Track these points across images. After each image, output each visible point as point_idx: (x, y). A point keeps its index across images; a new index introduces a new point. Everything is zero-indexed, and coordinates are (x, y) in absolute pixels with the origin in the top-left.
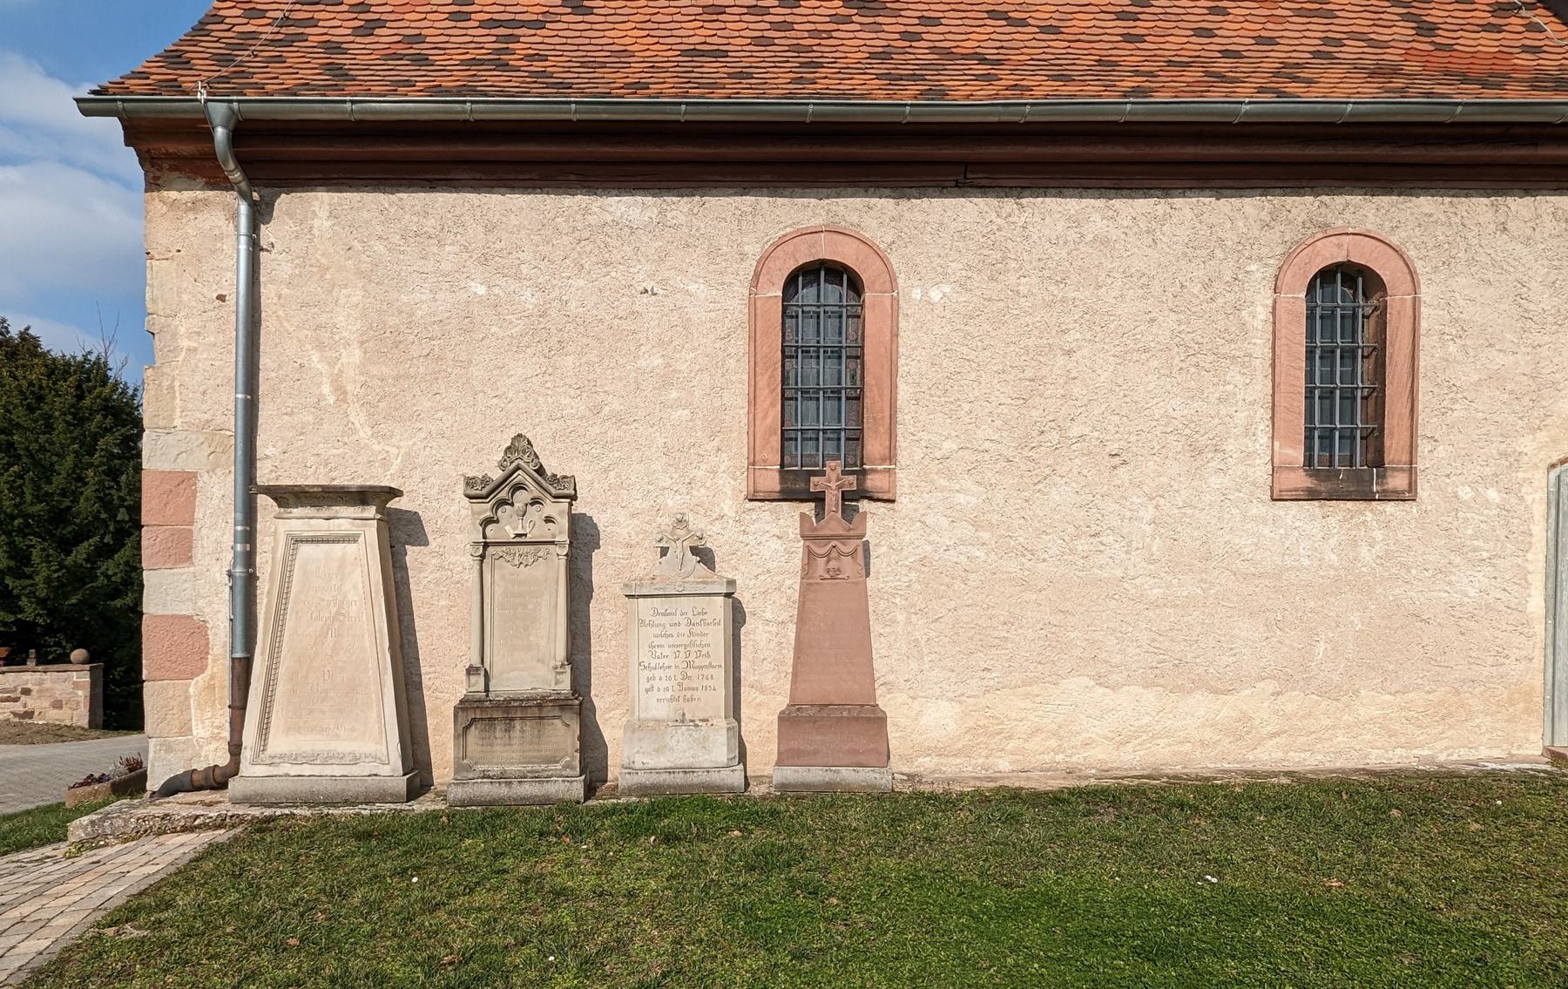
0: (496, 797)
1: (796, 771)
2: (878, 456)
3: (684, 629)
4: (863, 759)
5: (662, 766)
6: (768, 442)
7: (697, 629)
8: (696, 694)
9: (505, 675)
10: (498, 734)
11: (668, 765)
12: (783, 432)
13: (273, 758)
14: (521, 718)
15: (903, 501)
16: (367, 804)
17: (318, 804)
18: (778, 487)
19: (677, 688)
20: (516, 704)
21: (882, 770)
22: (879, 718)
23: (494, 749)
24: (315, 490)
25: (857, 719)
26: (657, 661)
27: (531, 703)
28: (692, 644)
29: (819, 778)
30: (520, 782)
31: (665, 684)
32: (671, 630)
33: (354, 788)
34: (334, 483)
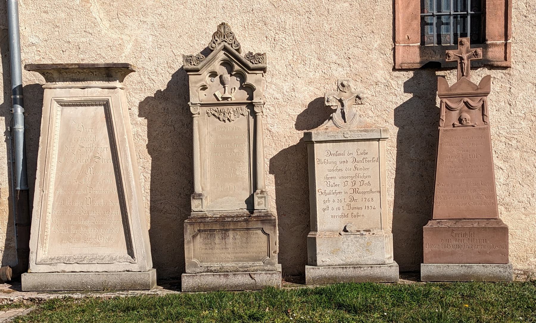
0: (217, 285)
1: (437, 267)
2: (497, 34)
3: (350, 165)
4: (490, 258)
5: (337, 263)
6: (410, 25)
7: (360, 165)
8: (361, 212)
9: (220, 200)
10: (217, 240)
11: (342, 262)
12: (422, 18)
13: (52, 259)
14: (234, 230)
15: (516, 68)
16: (123, 290)
17: (87, 291)
18: (418, 60)
19: (346, 208)
20: (230, 219)
21: (505, 265)
22: (502, 228)
23: (214, 251)
24: (73, 67)
25: (485, 228)
26: (331, 188)
27: (240, 219)
28: (357, 176)
29: (456, 271)
30: (234, 274)
31: (336, 205)
32: (340, 166)
33: (113, 280)
34: (84, 62)
